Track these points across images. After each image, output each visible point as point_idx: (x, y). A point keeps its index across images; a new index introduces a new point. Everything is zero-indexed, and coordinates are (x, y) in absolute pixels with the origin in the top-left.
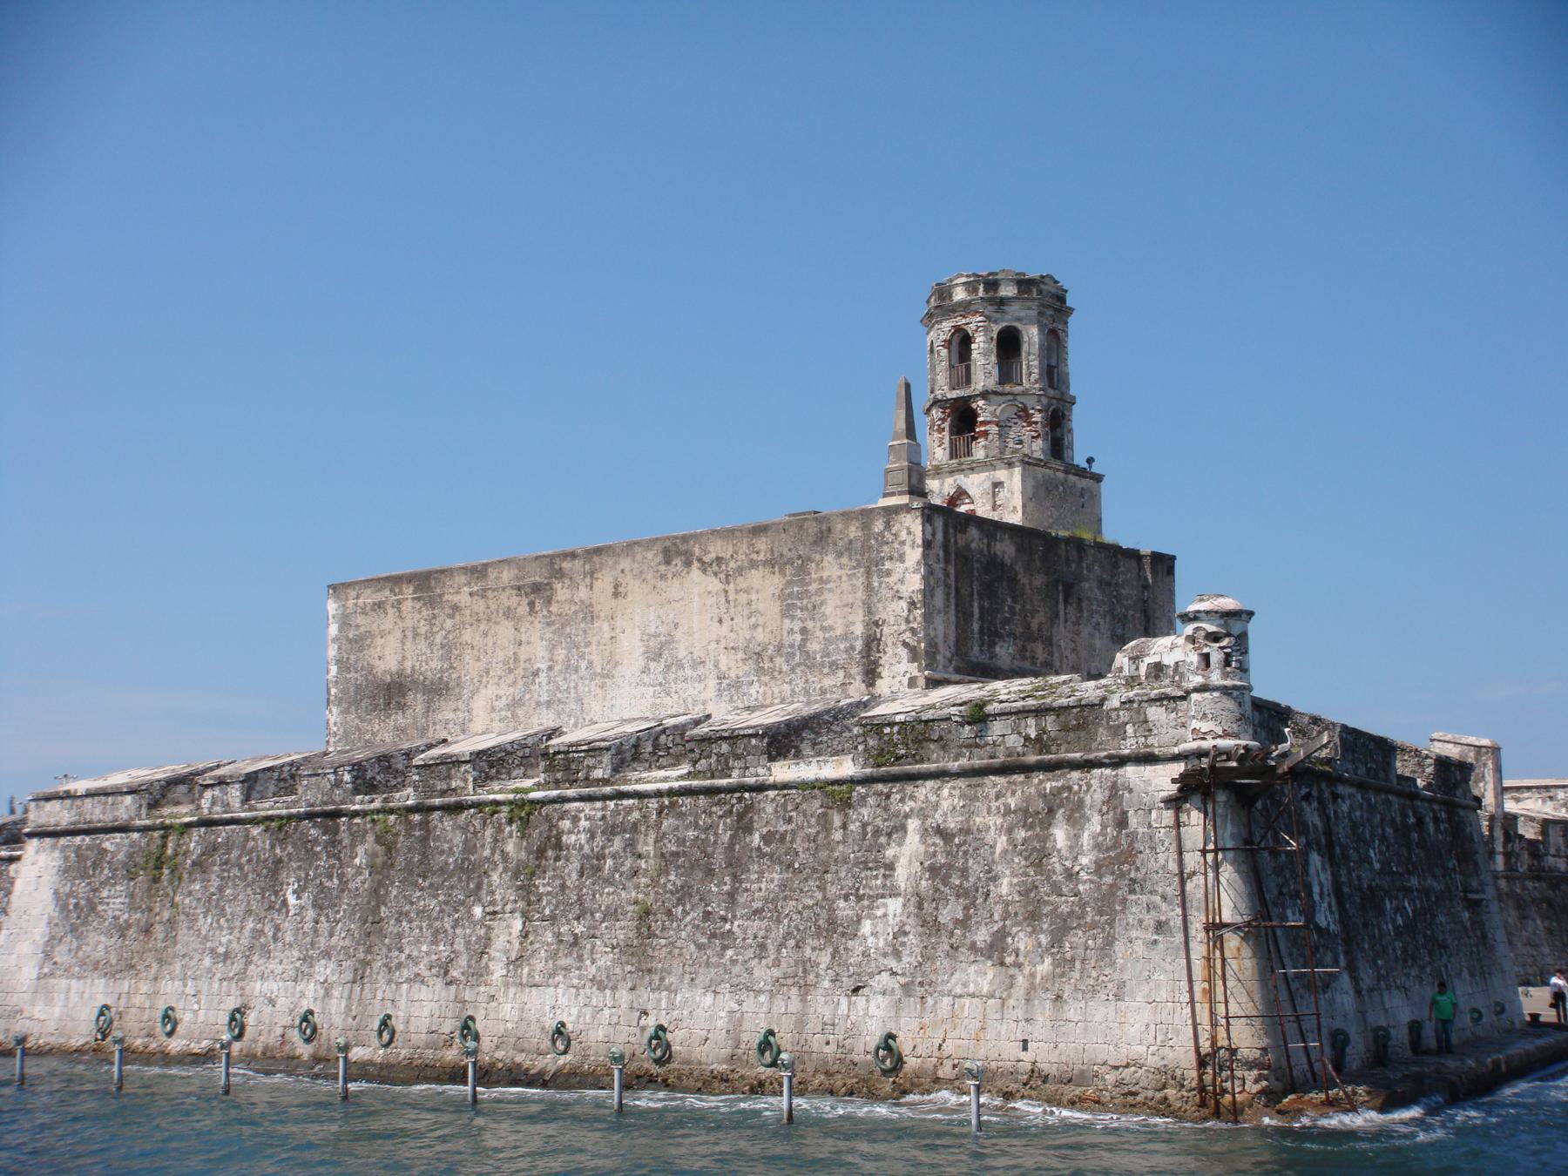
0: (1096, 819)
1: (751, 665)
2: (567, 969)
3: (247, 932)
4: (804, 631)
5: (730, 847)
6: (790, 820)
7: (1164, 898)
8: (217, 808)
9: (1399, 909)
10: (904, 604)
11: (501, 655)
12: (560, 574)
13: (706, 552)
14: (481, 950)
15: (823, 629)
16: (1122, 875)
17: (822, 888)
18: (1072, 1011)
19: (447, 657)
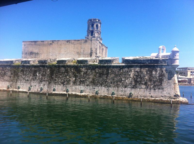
12: (53, 43)
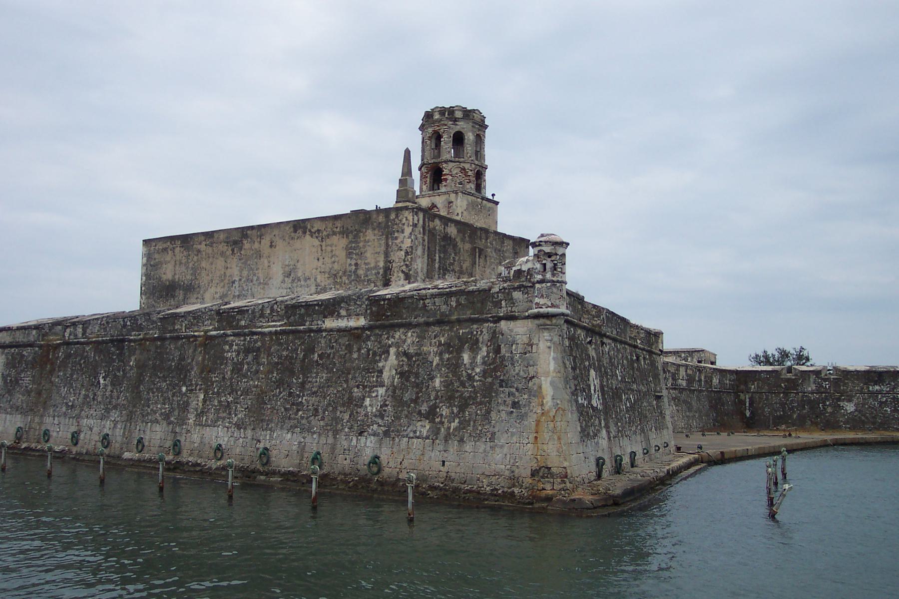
0: (485, 349)
1: (331, 280)
2: (224, 419)
3: (82, 396)
4: (356, 264)
5: (303, 361)
6: (332, 348)
7: (517, 390)
8: (72, 337)
9: (628, 399)
10: (403, 253)
11: (218, 274)
13: (313, 227)
14: (184, 407)
15: (365, 264)
16: (497, 377)
17: (347, 381)
18: (468, 447)
19: (194, 274)
